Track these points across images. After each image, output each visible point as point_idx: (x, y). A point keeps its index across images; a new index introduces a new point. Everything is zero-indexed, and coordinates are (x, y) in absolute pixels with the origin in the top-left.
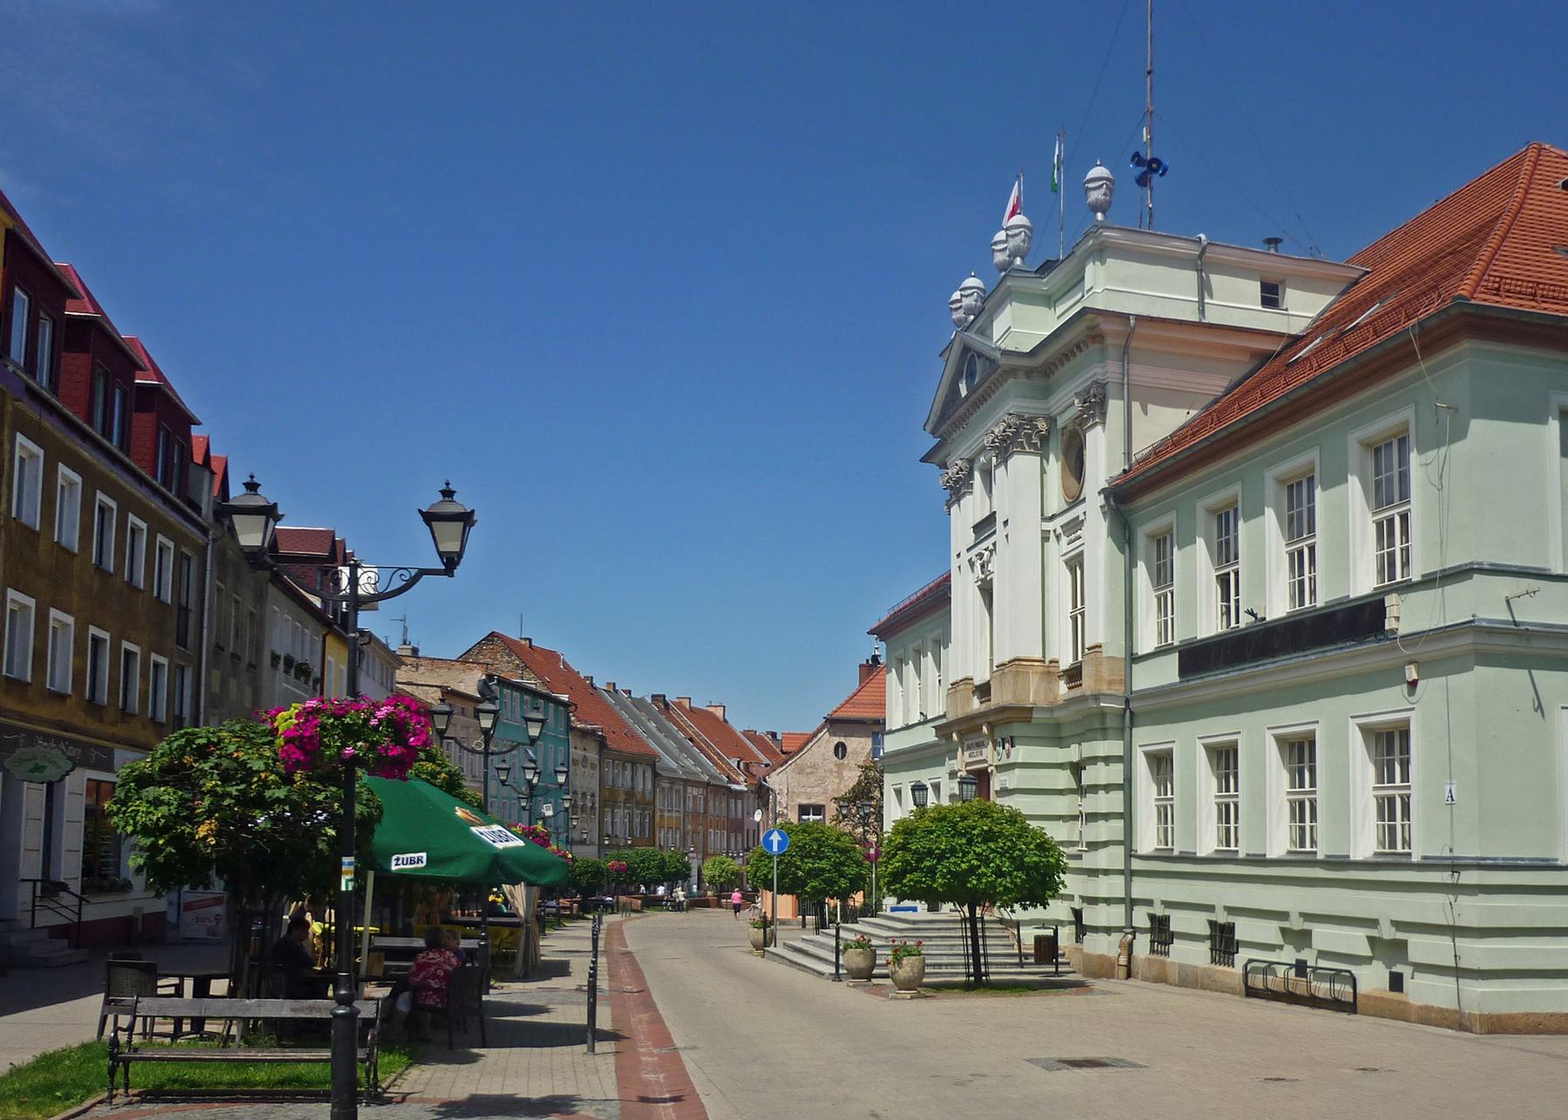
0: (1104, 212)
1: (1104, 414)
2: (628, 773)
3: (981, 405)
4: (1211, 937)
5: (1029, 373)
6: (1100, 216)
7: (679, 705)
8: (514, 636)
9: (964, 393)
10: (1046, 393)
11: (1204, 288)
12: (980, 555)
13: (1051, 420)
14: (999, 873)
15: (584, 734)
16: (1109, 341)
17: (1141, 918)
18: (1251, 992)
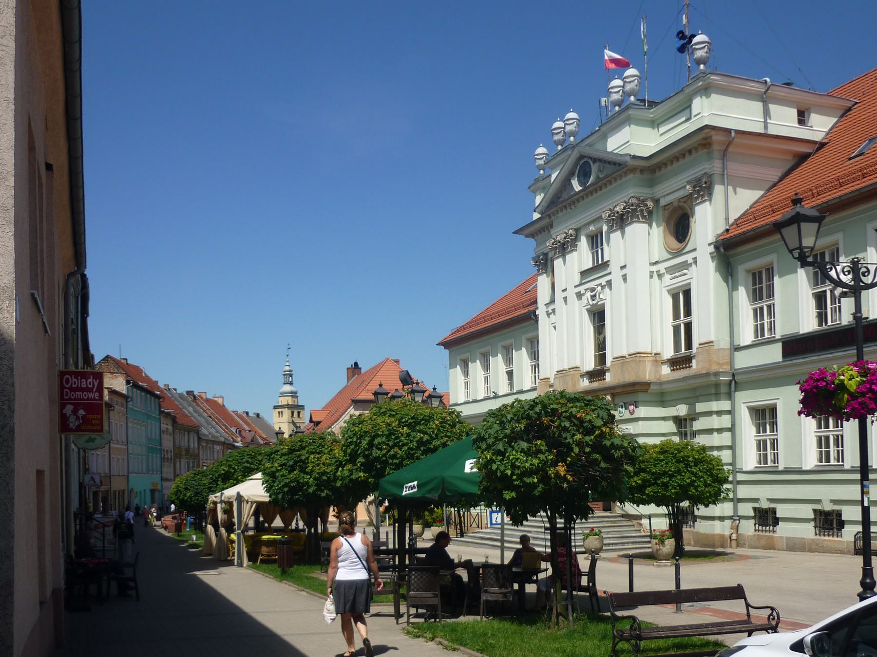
0: (704, 64)
1: (710, 195)
2: (186, 437)
3: (591, 190)
4: (814, 520)
5: (642, 170)
6: (702, 67)
7: (200, 396)
8: (117, 357)
11: (767, 114)
12: (593, 290)
13: (657, 201)
14: (706, 485)
15: (168, 414)
16: (715, 147)
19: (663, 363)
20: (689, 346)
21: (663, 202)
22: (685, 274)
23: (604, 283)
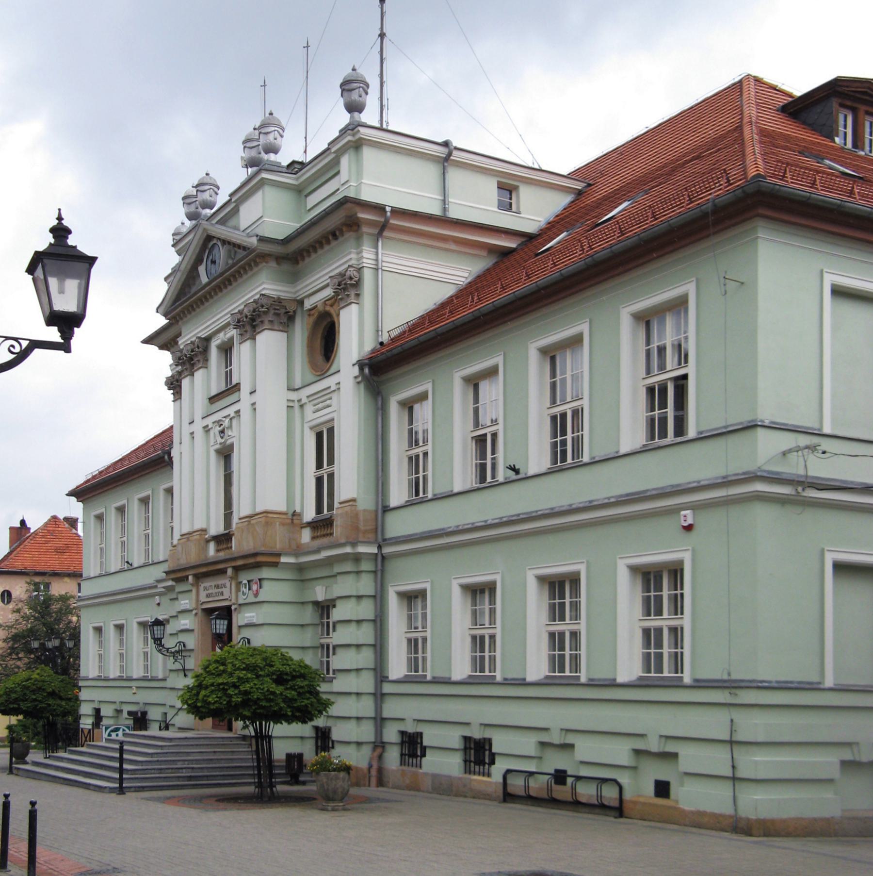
9: (204, 279)
10: (294, 277)
12: (219, 423)
17: (391, 734)
18: (508, 797)
19: (303, 526)
20: (331, 507)
21: (308, 304)
22: (329, 406)
23: (232, 415)
